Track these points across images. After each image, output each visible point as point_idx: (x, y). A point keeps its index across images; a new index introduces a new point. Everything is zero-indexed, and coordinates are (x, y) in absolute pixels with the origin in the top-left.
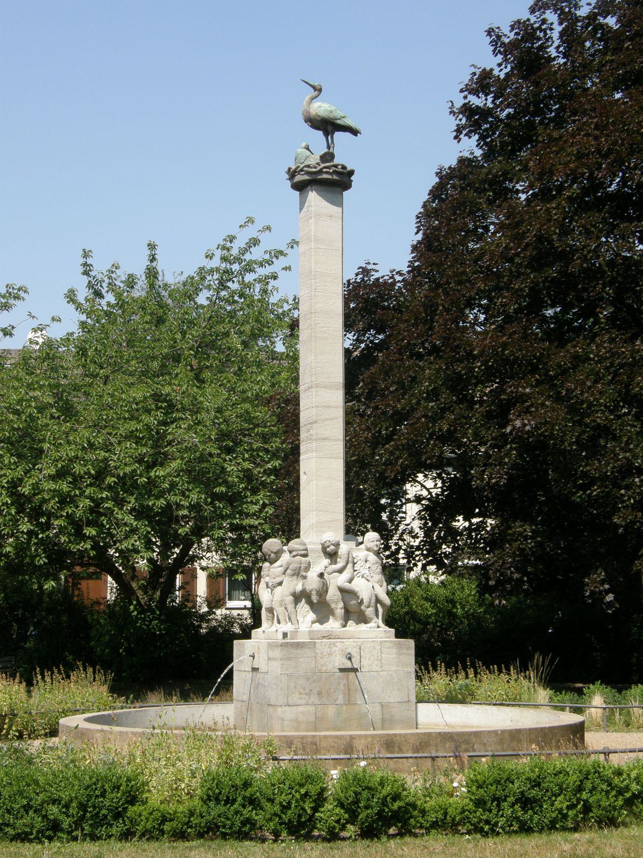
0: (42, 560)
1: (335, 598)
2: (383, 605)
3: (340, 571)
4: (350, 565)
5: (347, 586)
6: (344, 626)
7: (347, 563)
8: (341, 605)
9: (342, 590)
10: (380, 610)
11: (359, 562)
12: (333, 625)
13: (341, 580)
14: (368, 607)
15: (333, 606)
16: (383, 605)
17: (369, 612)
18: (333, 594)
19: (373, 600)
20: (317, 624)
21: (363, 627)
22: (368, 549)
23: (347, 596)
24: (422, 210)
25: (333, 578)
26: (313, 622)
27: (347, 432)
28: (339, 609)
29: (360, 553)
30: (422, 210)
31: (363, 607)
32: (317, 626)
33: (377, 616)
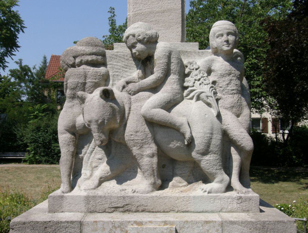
0: (132, 229)
1: (140, 136)
2: (240, 150)
3: (154, 88)
4: (173, 78)
5: (161, 114)
6: (162, 187)
7: (167, 73)
8: (152, 148)
9: (152, 123)
10: (236, 158)
11: (194, 72)
12: (140, 185)
13: (149, 104)
14: (205, 153)
15: (135, 151)
16: (240, 150)
17: (209, 162)
18: (134, 129)
19: (217, 140)
20: (113, 183)
21: (199, 189)
22: (216, 52)
23: (161, 134)
24: (111, 28)
25: (137, 101)
26: (102, 180)
27: (57, 127)
28: (147, 156)
29: (198, 59)
30: (111, 28)
31: (194, 154)
32: (112, 186)
33: (228, 170)
